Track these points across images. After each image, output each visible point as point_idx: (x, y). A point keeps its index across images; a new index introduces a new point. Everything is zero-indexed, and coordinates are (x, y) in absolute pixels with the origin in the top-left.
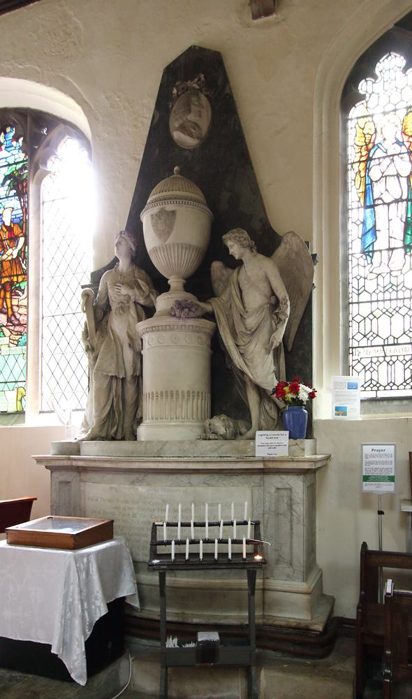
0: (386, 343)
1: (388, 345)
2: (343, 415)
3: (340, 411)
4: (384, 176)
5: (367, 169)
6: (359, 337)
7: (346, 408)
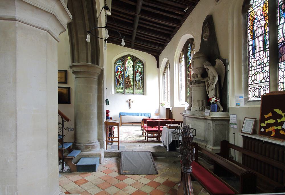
0: (266, 81)
1: (267, 82)
2: (238, 106)
3: (237, 105)
4: (258, 28)
5: (253, 27)
6: (251, 81)
7: (239, 104)
